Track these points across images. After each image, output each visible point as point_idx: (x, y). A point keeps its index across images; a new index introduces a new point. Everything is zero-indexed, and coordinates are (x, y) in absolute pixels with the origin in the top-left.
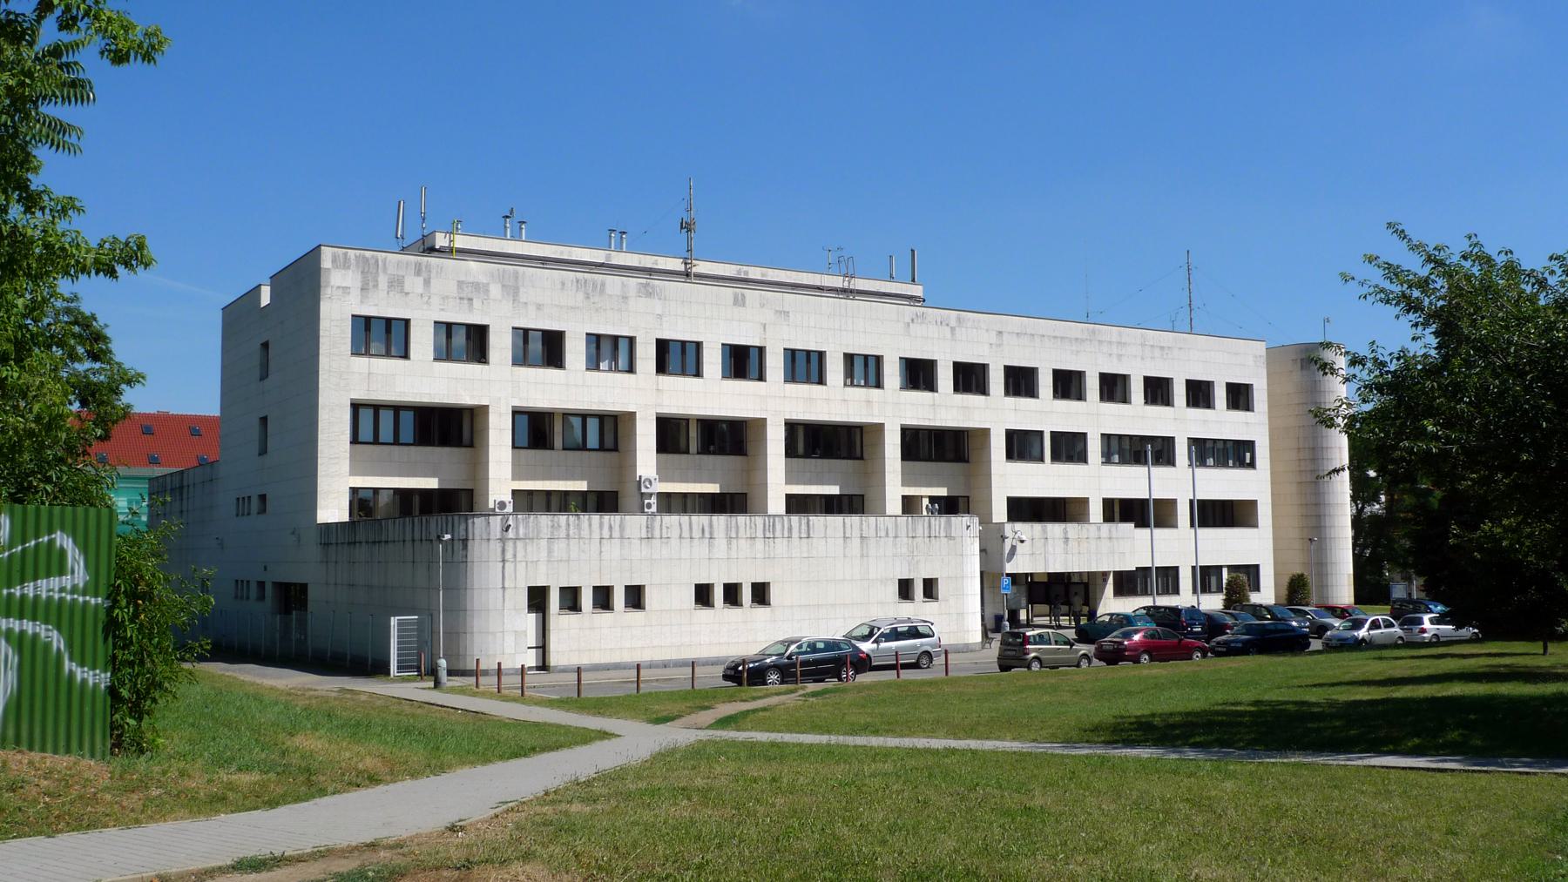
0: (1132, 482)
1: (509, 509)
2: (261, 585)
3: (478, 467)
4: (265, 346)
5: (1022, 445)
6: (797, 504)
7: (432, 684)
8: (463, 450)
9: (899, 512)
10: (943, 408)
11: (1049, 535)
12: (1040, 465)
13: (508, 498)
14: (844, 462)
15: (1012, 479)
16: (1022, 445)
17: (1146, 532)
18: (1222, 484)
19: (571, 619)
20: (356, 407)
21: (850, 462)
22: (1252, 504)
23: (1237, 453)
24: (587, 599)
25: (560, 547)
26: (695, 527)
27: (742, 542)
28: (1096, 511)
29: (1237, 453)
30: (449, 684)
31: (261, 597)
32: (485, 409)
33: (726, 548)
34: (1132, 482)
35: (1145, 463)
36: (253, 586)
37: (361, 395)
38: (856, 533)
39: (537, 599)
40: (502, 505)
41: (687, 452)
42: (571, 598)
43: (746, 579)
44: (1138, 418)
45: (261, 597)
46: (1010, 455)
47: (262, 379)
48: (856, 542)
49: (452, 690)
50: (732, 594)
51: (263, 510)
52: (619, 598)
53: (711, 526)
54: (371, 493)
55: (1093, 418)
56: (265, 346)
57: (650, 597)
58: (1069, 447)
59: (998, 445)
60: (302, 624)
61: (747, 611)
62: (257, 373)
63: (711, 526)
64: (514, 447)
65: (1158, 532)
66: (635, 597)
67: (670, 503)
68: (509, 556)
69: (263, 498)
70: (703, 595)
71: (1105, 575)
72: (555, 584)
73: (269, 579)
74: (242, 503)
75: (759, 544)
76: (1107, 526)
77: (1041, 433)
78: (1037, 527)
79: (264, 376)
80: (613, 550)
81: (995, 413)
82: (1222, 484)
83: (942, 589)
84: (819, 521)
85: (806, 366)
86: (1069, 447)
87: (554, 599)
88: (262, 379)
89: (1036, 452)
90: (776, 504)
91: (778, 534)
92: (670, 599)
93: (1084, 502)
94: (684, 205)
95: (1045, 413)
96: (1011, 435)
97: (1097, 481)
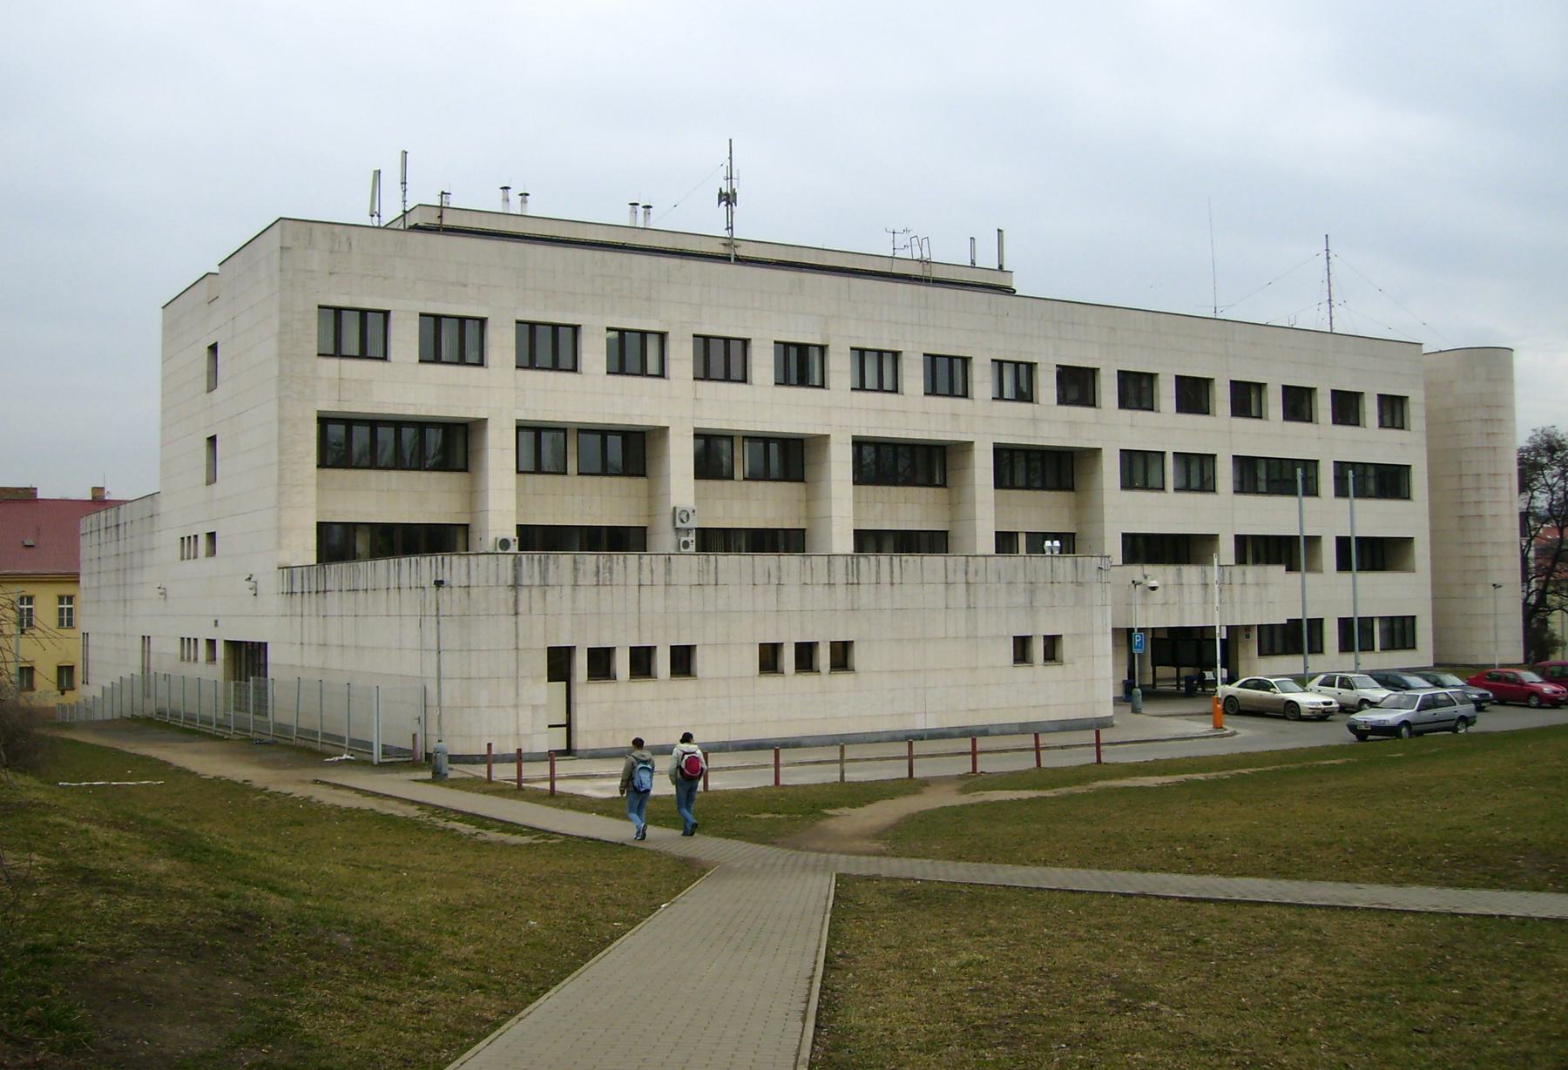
0: (1273, 515)
1: (514, 548)
2: (211, 643)
3: (474, 496)
4: (213, 349)
5: (1139, 469)
6: (867, 541)
7: (428, 775)
8: (455, 476)
9: (992, 551)
10: (1048, 424)
11: (1185, 581)
12: (1160, 495)
13: (512, 534)
14: (924, 490)
15: (1126, 512)
16: (1139, 469)
17: (1295, 577)
18: (1376, 518)
19: (601, 689)
20: (324, 421)
21: (931, 490)
22: (1406, 542)
23: (1388, 482)
24: (622, 663)
25: (586, 597)
26: (759, 571)
27: (819, 589)
28: (1227, 550)
29: (1388, 482)
30: (451, 775)
31: (212, 658)
32: (482, 422)
33: (791, 601)
34: (1273, 515)
35: (1294, 493)
36: (202, 646)
37: (330, 406)
38: (961, 577)
39: (559, 663)
40: (505, 544)
41: (732, 478)
42: (601, 663)
43: (823, 635)
44: (1272, 436)
45: (212, 658)
46: (1128, 483)
47: (210, 390)
48: (961, 588)
49: (456, 784)
50: (805, 656)
51: (212, 552)
52: (662, 663)
53: (779, 568)
54: (523, 434)
55: (1221, 435)
56: (213, 349)
57: (702, 662)
58: (1196, 472)
59: (1110, 469)
60: (262, 691)
61: (824, 681)
62: (203, 382)
63: (779, 568)
64: (518, 472)
65: (1310, 577)
66: (683, 661)
67: (712, 540)
68: (522, 608)
69: (212, 536)
70: (769, 658)
71: (1248, 628)
72: (583, 643)
73: (221, 637)
74: (188, 542)
75: (840, 591)
76: (1238, 570)
77: (1163, 453)
78: (1171, 570)
79: (212, 385)
80: (655, 601)
81: (1107, 429)
82: (1376, 518)
83: (1067, 649)
84: (731, 564)
85: (877, 369)
86: (1196, 472)
87: (581, 663)
88: (210, 390)
89: (1154, 479)
90: (843, 543)
91: (863, 579)
92: (727, 661)
93: (1212, 539)
94: (723, 172)
95: (1166, 430)
96: (1128, 457)
97: (1228, 514)
